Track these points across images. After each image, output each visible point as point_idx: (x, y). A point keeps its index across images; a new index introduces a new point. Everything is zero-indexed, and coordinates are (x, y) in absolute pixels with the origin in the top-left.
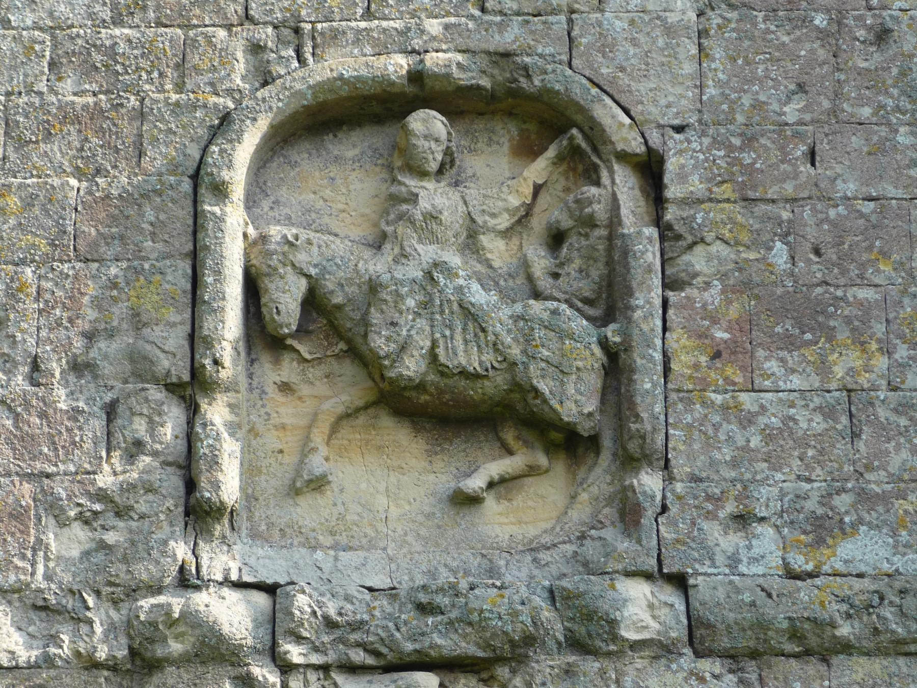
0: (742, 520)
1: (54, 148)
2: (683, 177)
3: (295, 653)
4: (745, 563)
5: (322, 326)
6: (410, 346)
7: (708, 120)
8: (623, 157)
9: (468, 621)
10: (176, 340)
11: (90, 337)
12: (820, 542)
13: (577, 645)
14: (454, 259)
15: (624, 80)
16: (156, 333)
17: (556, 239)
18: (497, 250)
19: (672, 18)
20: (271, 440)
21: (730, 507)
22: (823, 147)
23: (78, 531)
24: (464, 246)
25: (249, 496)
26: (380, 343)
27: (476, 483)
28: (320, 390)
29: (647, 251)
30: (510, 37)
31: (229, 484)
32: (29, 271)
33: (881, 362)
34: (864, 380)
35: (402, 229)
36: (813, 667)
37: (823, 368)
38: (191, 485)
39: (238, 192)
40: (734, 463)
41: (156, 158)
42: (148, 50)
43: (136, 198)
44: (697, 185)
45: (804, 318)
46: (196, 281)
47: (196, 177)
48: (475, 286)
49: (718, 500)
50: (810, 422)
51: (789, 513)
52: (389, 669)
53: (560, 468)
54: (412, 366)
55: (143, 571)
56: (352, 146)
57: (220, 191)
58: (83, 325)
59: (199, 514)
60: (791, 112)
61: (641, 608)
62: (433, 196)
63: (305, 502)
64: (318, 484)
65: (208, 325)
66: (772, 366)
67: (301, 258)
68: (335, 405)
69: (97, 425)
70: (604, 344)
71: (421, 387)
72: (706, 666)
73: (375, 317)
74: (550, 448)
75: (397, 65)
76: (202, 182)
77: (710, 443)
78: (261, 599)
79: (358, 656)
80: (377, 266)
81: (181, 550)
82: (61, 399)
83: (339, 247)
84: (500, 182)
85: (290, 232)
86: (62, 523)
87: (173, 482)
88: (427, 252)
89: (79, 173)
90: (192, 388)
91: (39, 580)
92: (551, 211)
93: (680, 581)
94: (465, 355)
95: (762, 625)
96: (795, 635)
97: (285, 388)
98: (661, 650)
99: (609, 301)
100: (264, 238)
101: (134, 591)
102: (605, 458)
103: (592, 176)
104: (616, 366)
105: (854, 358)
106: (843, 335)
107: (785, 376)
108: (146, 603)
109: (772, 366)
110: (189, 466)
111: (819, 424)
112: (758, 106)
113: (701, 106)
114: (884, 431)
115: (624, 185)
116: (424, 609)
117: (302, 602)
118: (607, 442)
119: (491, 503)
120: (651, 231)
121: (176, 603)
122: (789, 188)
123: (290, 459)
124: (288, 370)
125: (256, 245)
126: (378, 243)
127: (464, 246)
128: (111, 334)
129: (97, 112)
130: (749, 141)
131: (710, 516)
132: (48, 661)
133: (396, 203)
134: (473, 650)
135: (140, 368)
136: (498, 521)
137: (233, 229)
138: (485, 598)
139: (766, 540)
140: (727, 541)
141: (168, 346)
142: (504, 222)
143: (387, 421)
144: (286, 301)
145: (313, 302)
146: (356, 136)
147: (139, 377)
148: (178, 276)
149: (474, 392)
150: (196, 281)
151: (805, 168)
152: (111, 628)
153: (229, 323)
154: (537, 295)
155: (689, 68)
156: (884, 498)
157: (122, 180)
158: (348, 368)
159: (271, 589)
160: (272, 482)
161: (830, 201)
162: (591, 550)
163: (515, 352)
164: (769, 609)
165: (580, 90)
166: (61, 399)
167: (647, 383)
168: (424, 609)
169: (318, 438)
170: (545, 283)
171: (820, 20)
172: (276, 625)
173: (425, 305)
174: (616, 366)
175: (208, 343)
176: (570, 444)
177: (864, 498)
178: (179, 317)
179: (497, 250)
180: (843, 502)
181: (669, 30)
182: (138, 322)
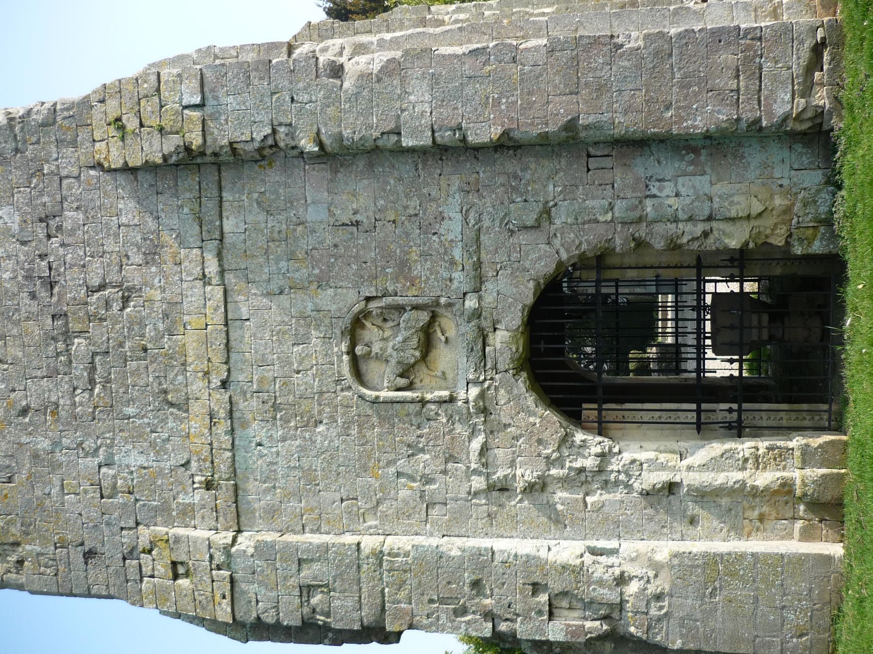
0: (451, 280)
1: (368, 435)
2: (371, 292)
3: (482, 378)
4: (460, 279)
5: (407, 373)
6: (412, 354)
7: (356, 286)
8: (366, 306)
9: (475, 341)
10: (412, 406)
11: (412, 425)
12: (455, 263)
13: (479, 317)
14: (391, 344)
15: (348, 305)
16: (411, 411)
17: (385, 320)
18: (388, 333)
19: (333, 294)
20: (433, 384)
21: (448, 283)
22: (363, 260)
23: (456, 426)
24: (388, 342)
25: (446, 389)
26: (412, 361)
27: (443, 338)
28: (422, 374)
29: (389, 300)
30: (338, 332)
31: (445, 393)
32: (397, 439)
33: (414, 248)
34: (418, 252)
35: (384, 356)
36: (483, 266)
37: (416, 261)
38: (445, 402)
39: (377, 393)
40: (438, 282)
41: (370, 412)
42: (343, 414)
43: (379, 416)
44: (373, 289)
45: (404, 266)
46: (398, 402)
47: (374, 403)
48: (397, 339)
49: (447, 285)
50: (428, 265)
51: (449, 269)
52: (485, 357)
53: (438, 319)
54: (417, 354)
55: (465, 411)
56: (363, 367)
57: (377, 397)
58: (409, 426)
59: (452, 400)
60: (354, 267)
61: (471, 303)
62: (376, 348)
63: (447, 376)
64: (444, 373)
65: (408, 399)
66: (415, 273)
67: (392, 379)
68: (425, 370)
69: (432, 422)
70: (411, 310)
71: (422, 351)
72: (483, 289)
73: (406, 362)
74: (434, 322)
75: (345, 358)
76: (375, 401)
77: (433, 287)
78: (470, 385)
79: (482, 364)
80: (393, 362)
81: (460, 403)
82: (426, 431)
83: (388, 370)
84: (371, 333)
85: (386, 381)
86: (454, 429)
87: (445, 406)
88: (390, 350)
89: (374, 429)
90: (423, 402)
91: (467, 433)
92: (379, 322)
93: (465, 294)
94: (414, 342)
95: (475, 277)
96: (476, 270)
97: (421, 381)
98: (480, 298)
99: (400, 309)
100: (388, 387)
101: (469, 413)
102: (437, 309)
103: (370, 313)
104: (416, 307)
105: (413, 254)
106: (408, 257)
107: (418, 270)
108: (472, 410)
109: (415, 273)
110: (441, 402)
111: (429, 263)
112: (353, 275)
113: (354, 288)
114: (430, 248)
115: (373, 305)
116: (472, 350)
117: (471, 377)
118: (433, 309)
119: (447, 335)
120: (384, 299)
121: (472, 404)
122: (373, 268)
123: (438, 380)
124: (417, 381)
125: (389, 389)
126: (387, 361)
127: (388, 342)
128: (411, 420)
129: (359, 426)
130: (362, 277)
131: (450, 287)
132: (484, 431)
133: (377, 357)
134: (481, 339)
135: (419, 414)
136: (451, 333)
137: (385, 394)
138: (470, 337)
139: (455, 275)
140: (456, 284)
141: (413, 408)
142: (381, 332)
143: (428, 358)
144: (402, 382)
145: (401, 376)
146: (361, 366)
147: (421, 414)
148: (397, 406)
149: (422, 339)
150: (398, 402)
151: (368, 264)
152: (477, 417)
153: (408, 394)
154: (399, 324)
155: (345, 291)
156: (445, 249)
157: (375, 419)
158: (416, 367)
159: (468, 383)
160: (444, 384)
161: (376, 259)
162: (458, 313)
163: (413, 330)
164: (471, 276)
165: (350, 316)
166: (426, 431)
167: (420, 301)
168: (472, 350)
169: (433, 374)
170: (396, 323)
171: (332, 260)
172: (476, 382)
173: (402, 351)
174: (416, 307)
175: (413, 399)
176: (434, 317)
177: (445, 253)
178: (407, 406)
179: (388, 333)
180: (446, 258)
181: (336, 295)
182: (408, 415)
